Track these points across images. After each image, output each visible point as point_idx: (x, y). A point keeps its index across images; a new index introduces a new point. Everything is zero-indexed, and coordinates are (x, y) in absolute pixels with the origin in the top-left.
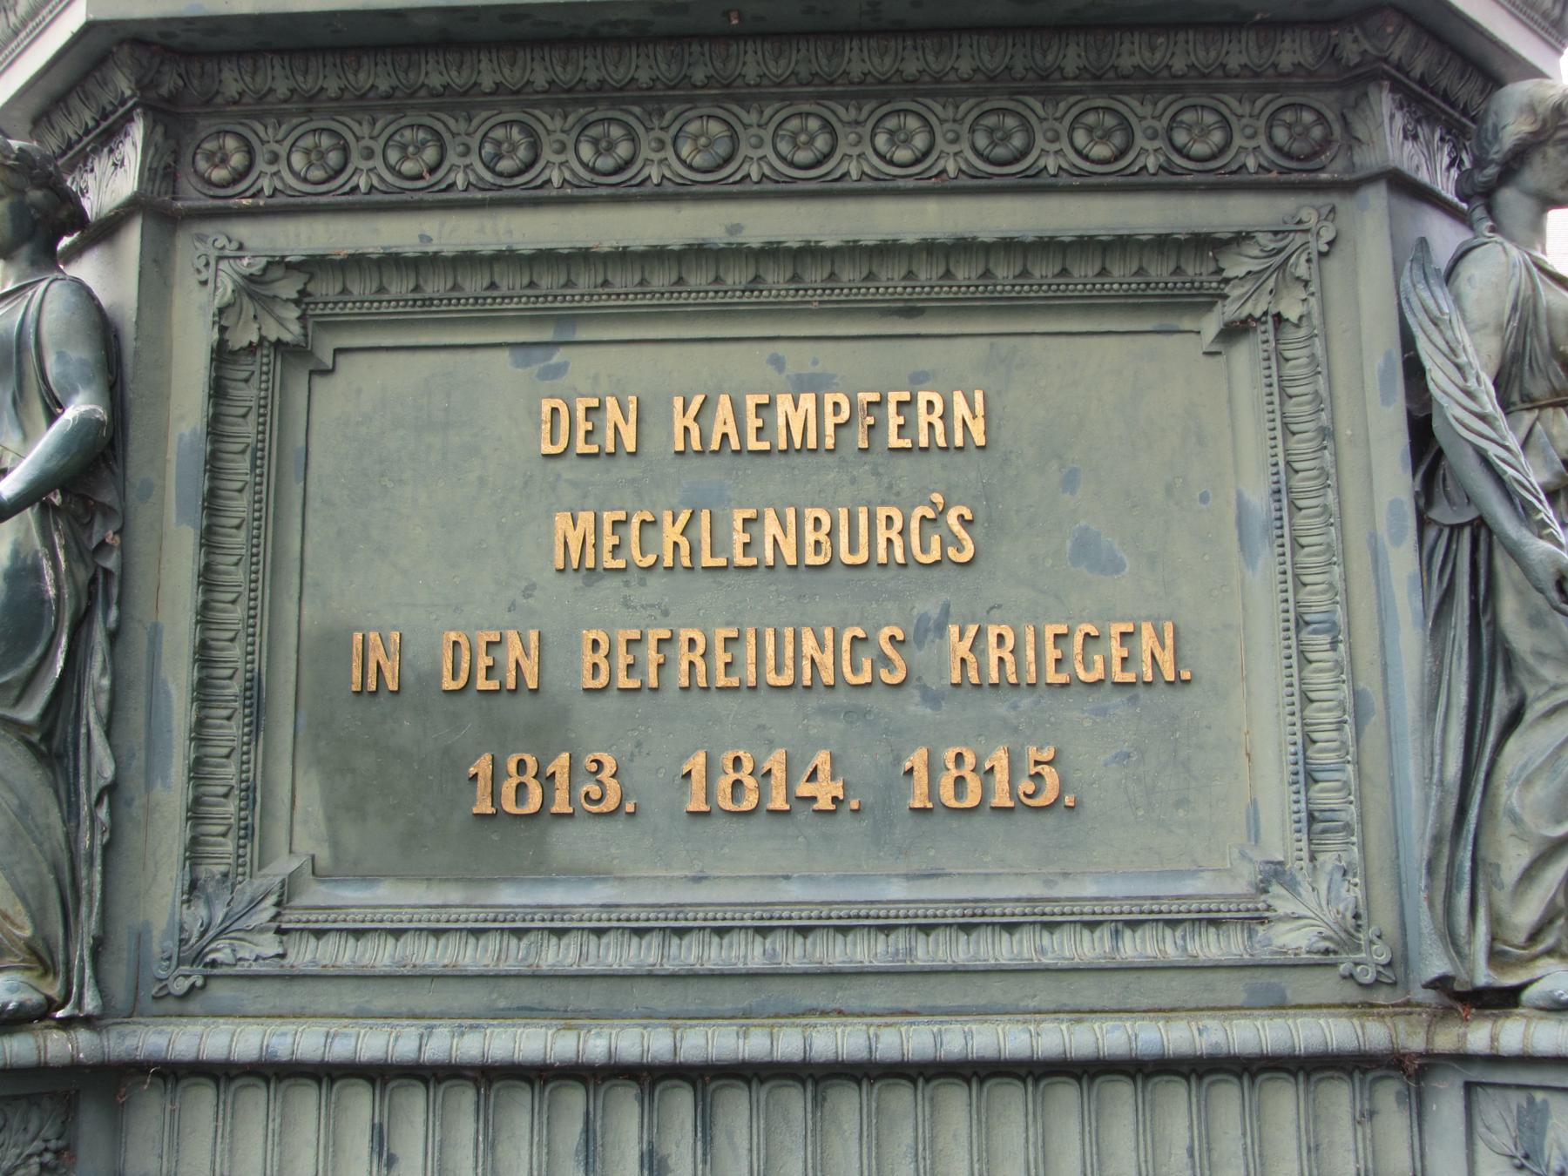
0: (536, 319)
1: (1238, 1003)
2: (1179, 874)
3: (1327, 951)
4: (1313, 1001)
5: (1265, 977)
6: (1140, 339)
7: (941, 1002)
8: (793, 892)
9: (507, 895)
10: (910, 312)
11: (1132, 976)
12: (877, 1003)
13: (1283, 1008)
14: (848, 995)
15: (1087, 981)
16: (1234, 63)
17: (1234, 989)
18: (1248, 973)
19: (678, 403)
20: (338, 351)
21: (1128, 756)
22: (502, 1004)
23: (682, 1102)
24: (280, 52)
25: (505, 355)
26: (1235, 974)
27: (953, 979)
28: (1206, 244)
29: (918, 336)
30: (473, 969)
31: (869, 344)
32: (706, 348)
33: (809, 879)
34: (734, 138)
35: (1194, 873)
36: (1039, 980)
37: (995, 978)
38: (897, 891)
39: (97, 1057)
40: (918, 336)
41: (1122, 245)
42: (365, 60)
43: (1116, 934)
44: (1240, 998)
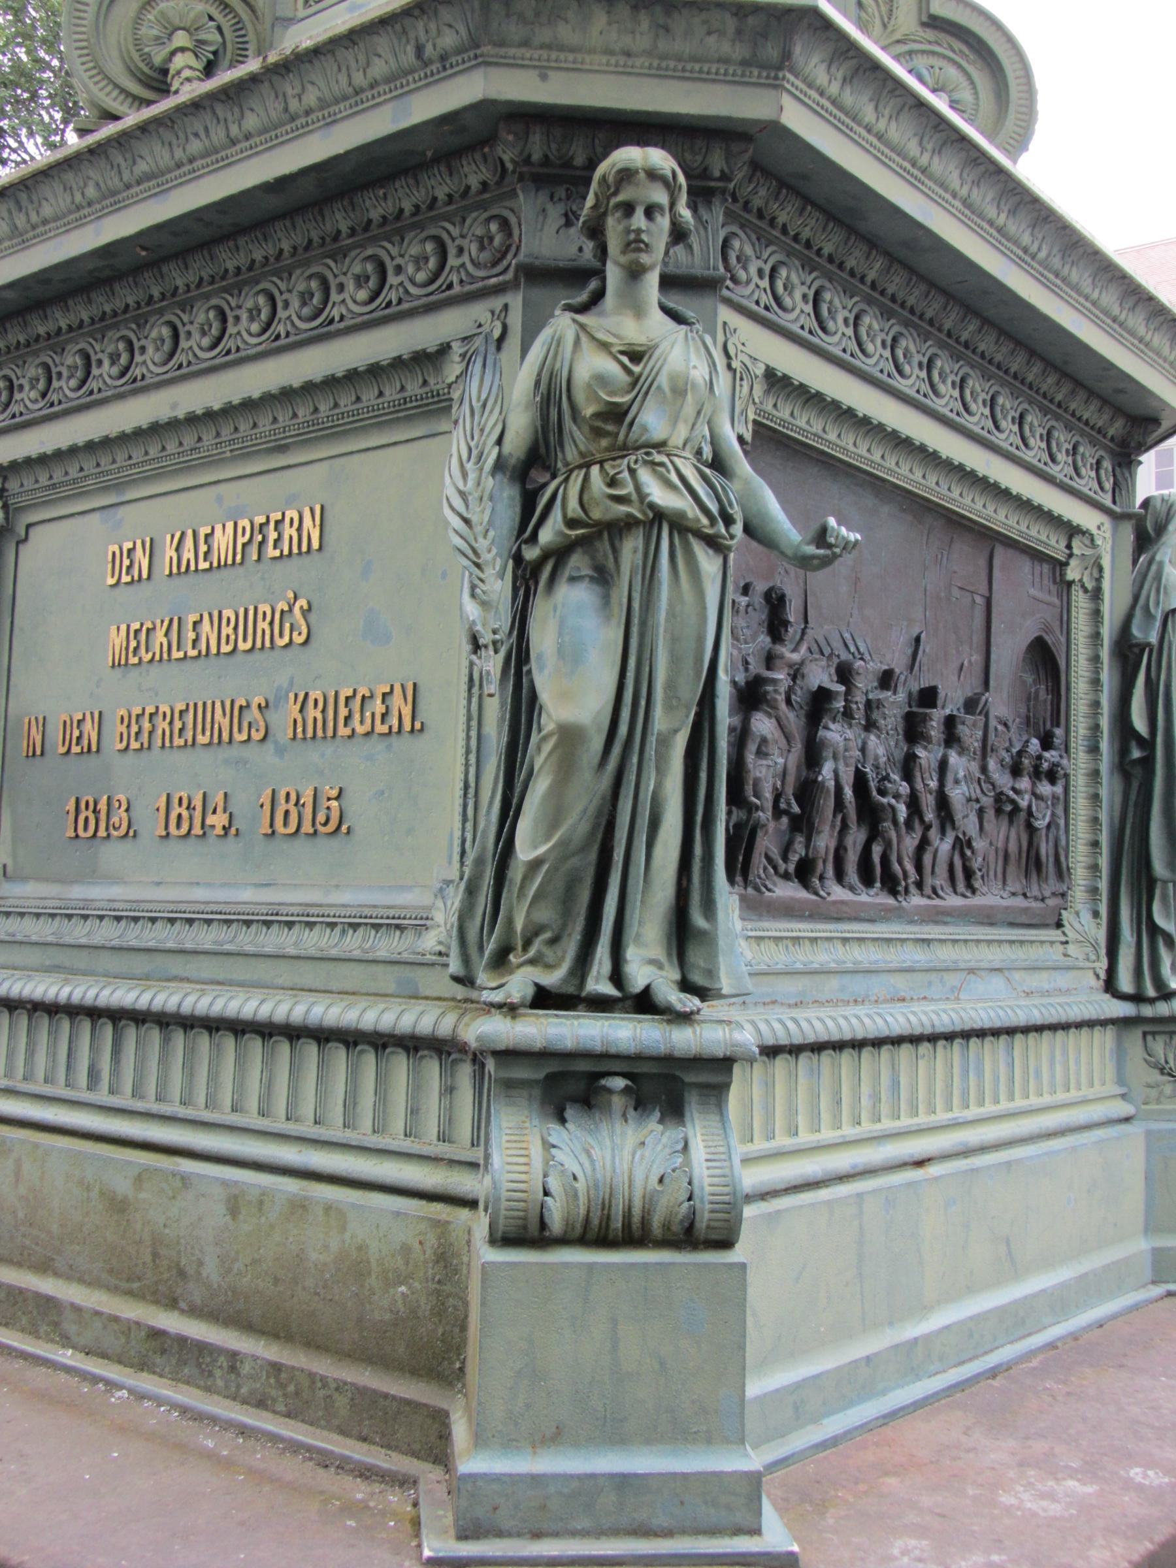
0: (106, 489)
1: (390, 991)
2: (402, 888)
3: (440, 954)
4: (435, 995)
5: (406, 972)
6: (416, 444)
7: (235, 976)
8: (200, 894)
9: (78, 892)
10: (282, 449)
11: (332, 965)
12: (205, 975)
13: (416, 997)
14: (190, 967)
15: (308, 966)
16: (441, 193)
17: (387, 979)
18: (396, 968)
19: (169, 537)
20: (29, 526)
21: (383, 793)
22: (48, 963)
23: (86, 1025)
24: (282, 216)
25: (95, 518)
26: (389, 968)
27: (241, 959)
28: (428, 360)
29: (289, 467)
30: (312, 952)
31: (272, 476)
32: (363, 455)
33: (209, 885)
34: (224, 319)
35: (409, 888)
36: (282, 963)
37: (261, 960)
38: (247, 895)
39: (663, 1049)
40: (289, 467)
41: (375, 371)
42: (8, 325)
43: (343, 932)
44: (392, 988)
